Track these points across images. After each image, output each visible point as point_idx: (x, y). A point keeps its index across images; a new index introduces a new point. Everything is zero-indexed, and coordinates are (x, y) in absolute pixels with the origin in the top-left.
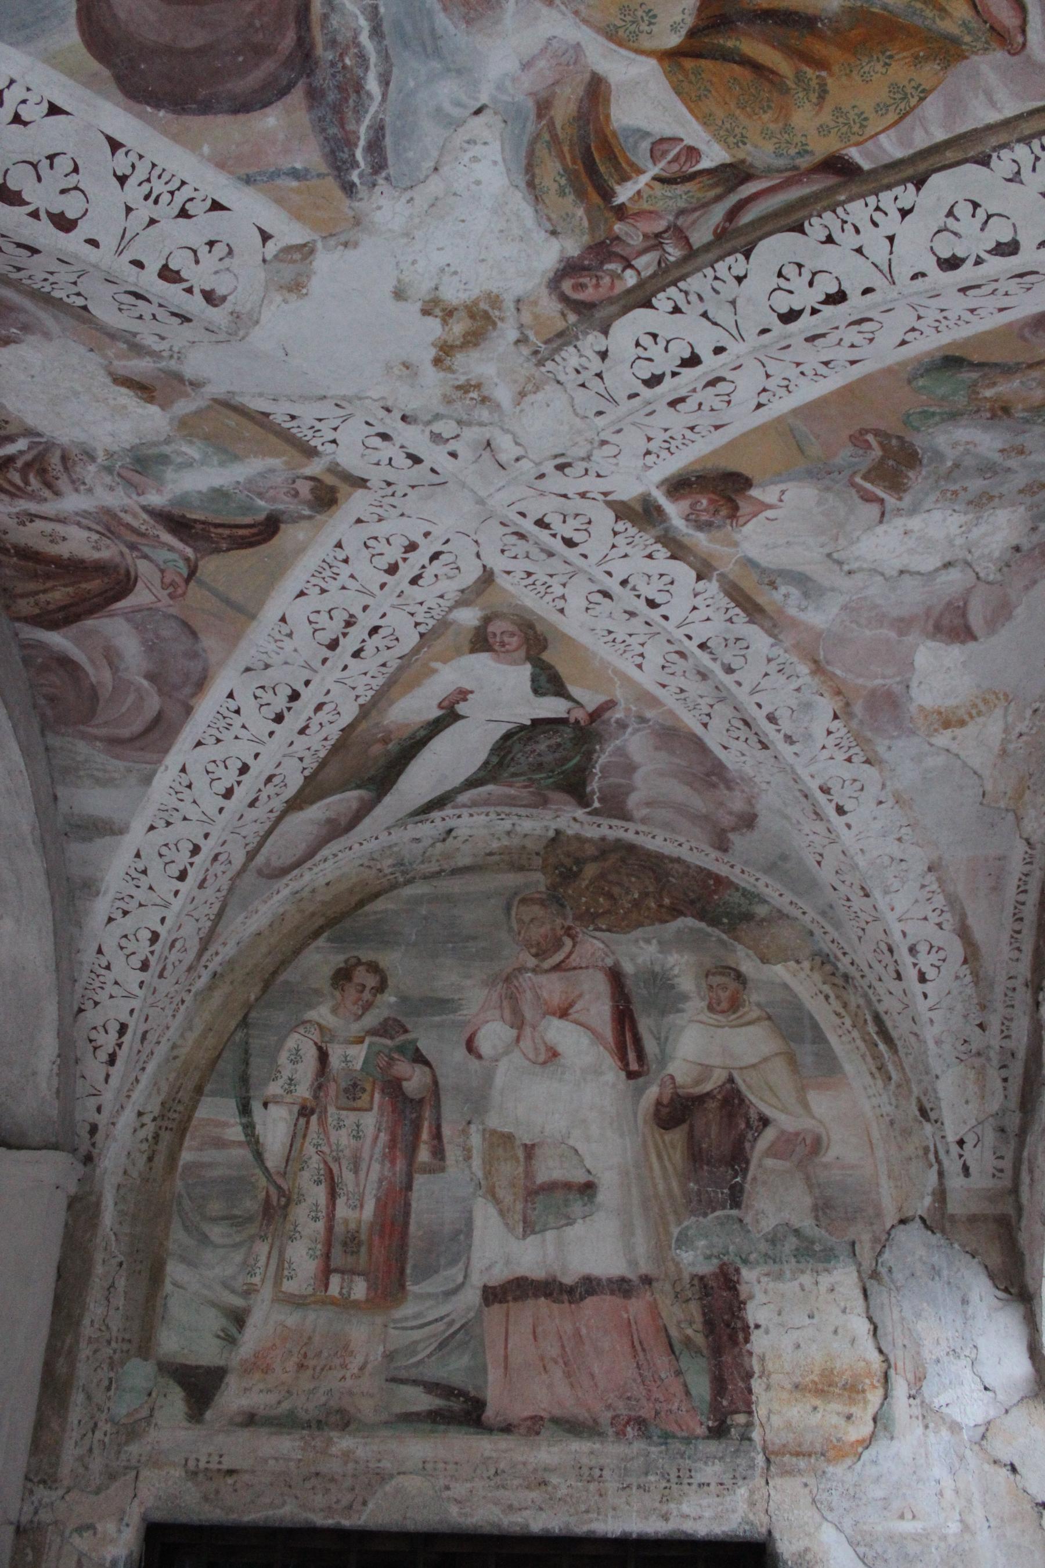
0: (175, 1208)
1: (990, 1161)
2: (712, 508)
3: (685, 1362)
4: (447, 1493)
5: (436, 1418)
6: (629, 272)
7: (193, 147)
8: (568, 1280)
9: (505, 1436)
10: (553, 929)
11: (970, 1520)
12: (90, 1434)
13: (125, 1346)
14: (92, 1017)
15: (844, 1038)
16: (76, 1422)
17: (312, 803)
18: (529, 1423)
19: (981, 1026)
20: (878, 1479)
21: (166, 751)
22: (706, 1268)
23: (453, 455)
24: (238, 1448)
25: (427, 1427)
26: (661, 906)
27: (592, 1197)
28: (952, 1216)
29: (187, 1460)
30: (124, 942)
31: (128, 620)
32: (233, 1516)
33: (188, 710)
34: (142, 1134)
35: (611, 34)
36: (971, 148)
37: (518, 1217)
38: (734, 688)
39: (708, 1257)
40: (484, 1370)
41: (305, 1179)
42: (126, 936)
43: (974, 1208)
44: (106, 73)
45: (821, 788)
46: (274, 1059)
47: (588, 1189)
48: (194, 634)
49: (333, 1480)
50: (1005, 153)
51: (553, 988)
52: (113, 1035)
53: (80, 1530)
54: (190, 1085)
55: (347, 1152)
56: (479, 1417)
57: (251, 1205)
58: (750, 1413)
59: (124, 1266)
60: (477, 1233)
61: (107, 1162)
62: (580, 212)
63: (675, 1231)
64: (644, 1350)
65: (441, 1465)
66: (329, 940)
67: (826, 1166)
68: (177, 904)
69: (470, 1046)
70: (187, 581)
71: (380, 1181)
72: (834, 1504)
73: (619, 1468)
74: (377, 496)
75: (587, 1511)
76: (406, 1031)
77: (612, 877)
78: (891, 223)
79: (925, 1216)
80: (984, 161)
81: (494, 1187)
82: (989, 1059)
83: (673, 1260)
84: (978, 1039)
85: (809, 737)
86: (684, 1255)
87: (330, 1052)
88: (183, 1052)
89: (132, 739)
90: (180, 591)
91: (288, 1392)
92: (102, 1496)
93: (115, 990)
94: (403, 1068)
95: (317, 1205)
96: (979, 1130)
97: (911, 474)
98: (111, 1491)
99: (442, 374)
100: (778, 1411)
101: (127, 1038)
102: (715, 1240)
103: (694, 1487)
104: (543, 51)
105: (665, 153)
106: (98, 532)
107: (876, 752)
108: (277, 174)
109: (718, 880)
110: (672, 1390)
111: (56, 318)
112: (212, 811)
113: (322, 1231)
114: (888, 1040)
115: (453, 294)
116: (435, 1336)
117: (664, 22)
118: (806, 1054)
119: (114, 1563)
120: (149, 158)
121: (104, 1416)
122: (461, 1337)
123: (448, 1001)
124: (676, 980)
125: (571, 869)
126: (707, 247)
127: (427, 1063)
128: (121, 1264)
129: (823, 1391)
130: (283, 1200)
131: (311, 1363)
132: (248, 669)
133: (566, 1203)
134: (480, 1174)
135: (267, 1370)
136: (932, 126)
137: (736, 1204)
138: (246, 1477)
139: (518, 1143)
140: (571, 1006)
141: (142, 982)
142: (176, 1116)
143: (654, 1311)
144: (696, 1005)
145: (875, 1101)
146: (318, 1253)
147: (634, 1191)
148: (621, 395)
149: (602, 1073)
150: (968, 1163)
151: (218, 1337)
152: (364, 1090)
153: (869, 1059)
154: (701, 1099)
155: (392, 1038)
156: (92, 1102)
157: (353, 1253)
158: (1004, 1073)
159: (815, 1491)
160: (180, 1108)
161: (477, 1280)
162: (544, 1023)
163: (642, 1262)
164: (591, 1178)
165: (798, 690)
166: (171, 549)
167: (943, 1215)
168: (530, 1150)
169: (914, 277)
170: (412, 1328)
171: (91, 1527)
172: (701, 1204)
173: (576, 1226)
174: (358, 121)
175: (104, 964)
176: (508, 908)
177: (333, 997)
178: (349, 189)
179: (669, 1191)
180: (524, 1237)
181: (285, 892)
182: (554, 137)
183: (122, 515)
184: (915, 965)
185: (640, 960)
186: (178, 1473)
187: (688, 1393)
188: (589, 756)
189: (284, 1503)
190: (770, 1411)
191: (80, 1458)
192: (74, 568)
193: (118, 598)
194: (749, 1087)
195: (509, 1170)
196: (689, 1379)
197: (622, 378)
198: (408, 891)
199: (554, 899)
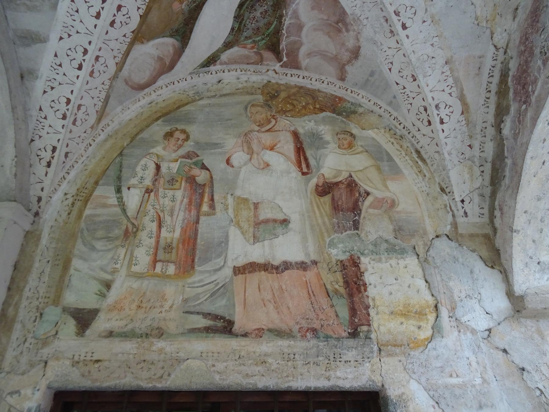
0: (79, 235)
1: (477, 210)
3: (335, 301)
4: (214, 368)
5: (208, 330)
8: (276, 263)
9: (244, 339)
10: (267, 116)
11: (486, 377)
12: (22, 345)
13: (46, 300)
14: (38, 144)
15: (402, 160)
16: (15, 339)
17: (148, 40)
18: (256, 332)
19: (470, 146)
20: (437, 357)
22: (344, 257)
24: (103, 349)
25: (204, 335)
26: (315, 108)
27: (287, 226)
28: (461, 234)
29: (74, 355)
30: (53, 104)
32: (98, 384)
34: (66, 203)
37: (251, 235)
39: (344, 252)
40: (234, 305)
41: (146, 220)
42: (53, 101)
43: (472, 230)
45: (395, 12)
46: (134, 169)
47: (285, 222)
49: (153, 363)
51: (267, 139)
52: (49, 152)
53: (11, 394)
54: (92, 180)
55: (168, 208)
56: (231, 329)
57: (117, 232)
58: (369, 325)
59: (50, 262)
60: (230, 243)
61: (47, 216)
63: (328, 240)
64: (314, 295)
65: (210, 354)
66: (163, 121)
67: (398, 212)
68: (79, 83)
69: (228, 162)
71: (184, 220)
72: (415, 370)
73: (304, 354)
75: (287, 376)
76: (198, 156)
77: (293, 98)
79: (448, 234)
81: (239, 221)
82: (473, 162)
83: (327, 253)
84: (468, 153)
86: (333, 251)
87: (161, 165)
88: (90, 167)
91: (131, 320)
92: (25, 376)
93: (51, 130)
94: (196, 171)
95: (152, 231)
96: (471, 195)
98: (31, 373)
100: (383, 325)
101: (56, 154)
102: (347, 244)
103: (343, 363)
109: (341, 99)
110: (329, 314)
112: (91, 28)
113: (154, 244)
114: (423, 160)
116: (209, 290)
118: (385, 166)
119: (29, 411)
121: (31, 335)
122: (222, 290)
123: (217, 144)
124: (323, 136)
125: (274, 94)
127: (208, 169)
128: (48, 262)
129: (405, 314)
130: (135, 230)
131: (144, 305)
133: (274, 228)
134: (232, 216)
135: (121, 309)
137: (357, 228)
138: (106, 364)
139: (250, 202)
140: (275, 146)
141: (64, 126)
142: (84, 194)
143: (318, 275)
144: (333, 146)
145: (419, 185)
146: (151, 253)
147: (307, 222)
149: (290, 173)
150: (467, 211)
151: (97, 294)
152: (177, 181)
153: (414, 168)
154: (337, 184)
155: (191, 159)
156: (39, 186)
157: (168, 253)
158: (482, 169)
159: (405, 364)
160: (86, 191)
161: (231, 264)
162: (262, 152)
163: (312, 255)
164: (286, 217)
167: (457, 234)
168: (256, 206)
170: (197, 287)
171: (18, 392)
172: (340, 228)
173: (279, 238)
175: (43, 116)
176: (246, 108)
177: (164, 144)
179: (324, 223)
180: (254, 244)
181: (143, 102)
184: (438, 115)
185: (306, 128)
186: (68, 363)
187: (337, 316)
188: (280, 23)
189: (126, 376)
190: (379, 325)
191: (16, 357)
194: (359, 179)
195: (245, 214)
196: (338, 309)
198: (201, 102)
199: (267, 105)
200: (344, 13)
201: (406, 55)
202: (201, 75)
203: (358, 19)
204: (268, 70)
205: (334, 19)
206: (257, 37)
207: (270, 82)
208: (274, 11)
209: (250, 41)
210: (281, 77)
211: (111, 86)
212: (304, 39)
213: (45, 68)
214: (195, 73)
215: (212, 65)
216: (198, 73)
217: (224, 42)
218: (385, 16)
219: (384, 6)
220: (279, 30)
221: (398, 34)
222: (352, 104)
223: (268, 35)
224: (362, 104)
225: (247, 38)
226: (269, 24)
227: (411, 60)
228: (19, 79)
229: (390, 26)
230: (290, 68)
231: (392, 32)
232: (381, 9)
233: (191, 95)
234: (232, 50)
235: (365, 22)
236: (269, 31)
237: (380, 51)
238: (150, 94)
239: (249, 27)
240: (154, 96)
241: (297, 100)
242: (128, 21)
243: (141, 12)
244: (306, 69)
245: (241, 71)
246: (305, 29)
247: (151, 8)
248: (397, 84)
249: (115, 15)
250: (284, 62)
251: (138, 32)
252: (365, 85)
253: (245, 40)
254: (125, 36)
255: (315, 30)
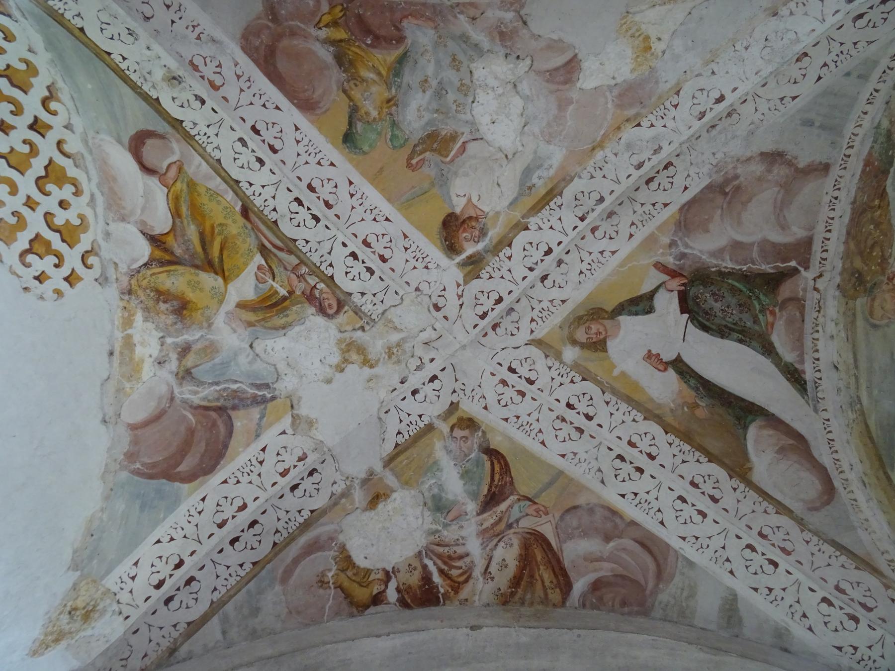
2: (470, 230)
6: (318, 286)
7: (238, 453)
10: (889, 291)
17: (747, 459)
21: (668, 546)
23: (432, 360)
31: (565, 542)
33: (633, 523)
35: (221, 302)
36: (217, 166)
38: (614, 195)
44: (201, 479)
45: (700, 119)
48: (575, 508)
50: (213, 155)
62: (294, 308)
70: (535, 503)
74: (465, 398)
78: (257, 188)
80: (219, 161)
85: (655, 138)
89: (658, 565)
90: (542, 508)
97: (443, 133)
99: (380, 364)
104: (229, 325)
105: (262, 278)
106: (499, 541)
107: (670, 89)
108: (259, 425)
111: (322, 525)
115: (336, 359)
117: (214, 284)
120: (234, 470)
126: (298, 257)
132: (603, 482)
136: (216, 183)
148: (383, 285)
165: (616, 155)
166: (511, 507)
169: (274, 173)
174: (247, 392)
176: (875, 326)
178: (273, 398)
182: (263, 319)
183: (484, 527)
188: (731, 274)
192: (526, 560)
193: (549, 544)
197: (373, 285)
198: (865, 400)
199: (871, 290)
200: (709, 188)
201: (763, 83)
202: (819, 395)
203: (716, 166)
204: (815, 289)
205: (720, 200)
206: (754, 307)
207: (839, 286)
208: (712, 284)
209: (761, 317)
210: (828, 267)
211: (816, 533)
212: (757, 237)
213: (778, 615)
214: (816, 404)
215: (803, 375)
216: (817, 400)
217: (763, 354)
218: (708, 131)
219: (692, 136)
220: (743, 274)
221: (731, 105)
222: (875, 141)
223: (750, 290)
224: (875, 124)
225: (756, 321)
226: (733, 290)
227: (771, 73)
228: (786, 655)
229: (720, 119)
230: (810, 254)
231: (729, 115)
232: (697, 139)
233: (855, 416)
234: (777, 344)
235: (719, 156)
236: (744, 290)
237: (765, 122)
238: (847, 480)
239: (737, 319)
240: (852, 476)
241: (867, 238)
242: (713, 479)
243: (703, 459)
244: (812, 228)
245: (817, 331)
246: (739, 238)
247: (700, 446)
248: (820, 78)
249: (703, 493)
250: (799, 264)
251: (732, 470)
252: (832, 129)
253: (760, 324)
254: (735, 489)
255: (740, 223)
